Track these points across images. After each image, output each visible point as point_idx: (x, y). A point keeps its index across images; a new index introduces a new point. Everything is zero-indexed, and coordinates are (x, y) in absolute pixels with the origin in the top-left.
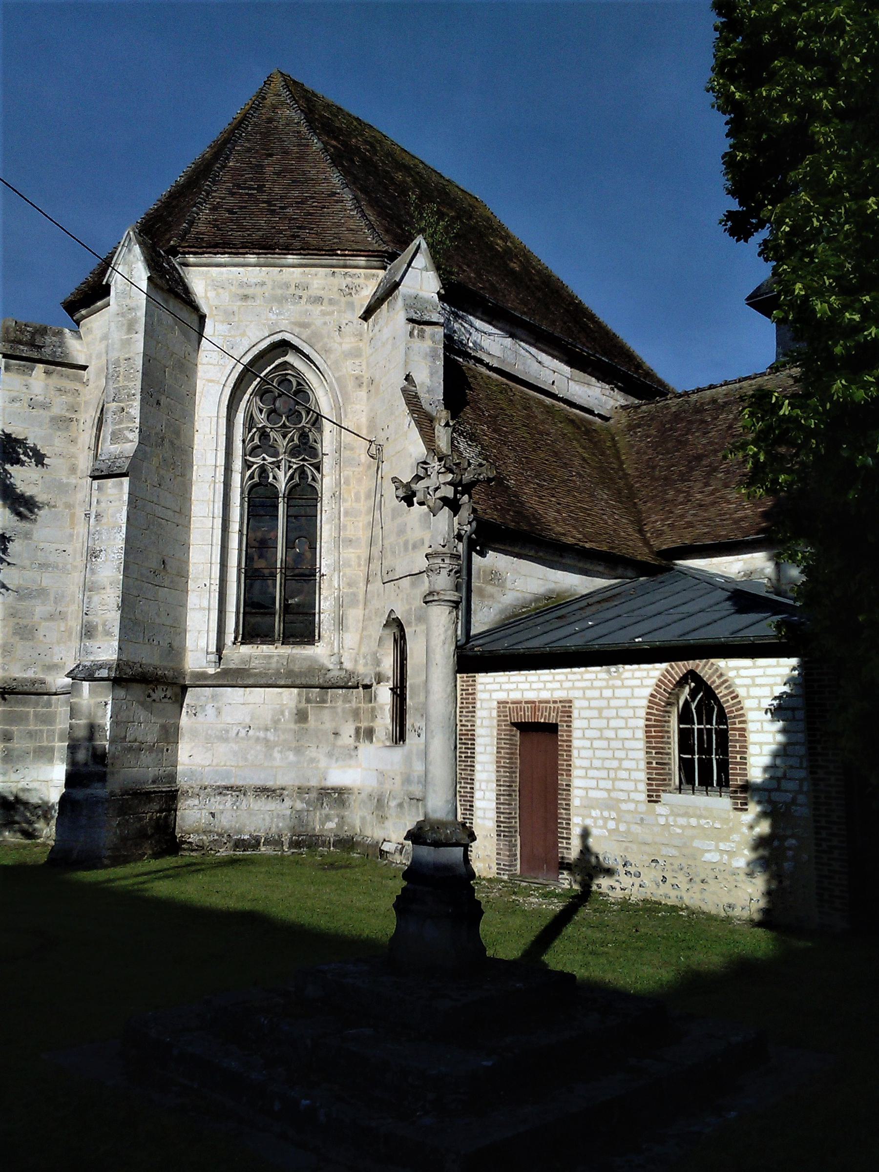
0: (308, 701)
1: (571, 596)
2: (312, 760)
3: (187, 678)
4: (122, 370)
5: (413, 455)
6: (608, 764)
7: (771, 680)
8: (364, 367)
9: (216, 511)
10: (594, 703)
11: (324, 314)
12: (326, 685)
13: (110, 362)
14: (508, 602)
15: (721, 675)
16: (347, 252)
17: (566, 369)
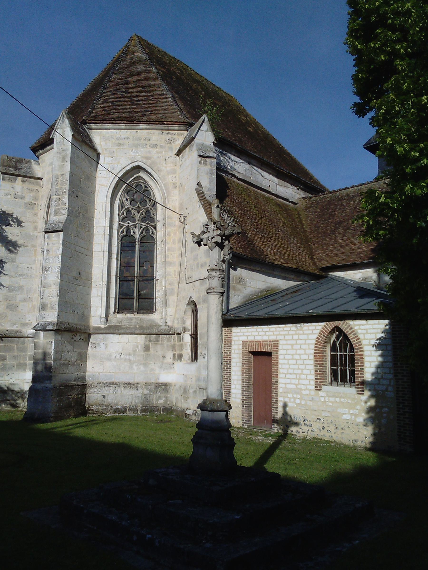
0: (150, 341)
2: (152, 370)
3: (91, 330)
4: (59, 180)
6: (296, 371)
7: (376, 331)
8: (177, 178)
10: (289, 342)
11: (158, 152)
12: (159, 333)
14: (247, 293)
15: (351, 328)
16: (169, 123)
17: (276, 180)
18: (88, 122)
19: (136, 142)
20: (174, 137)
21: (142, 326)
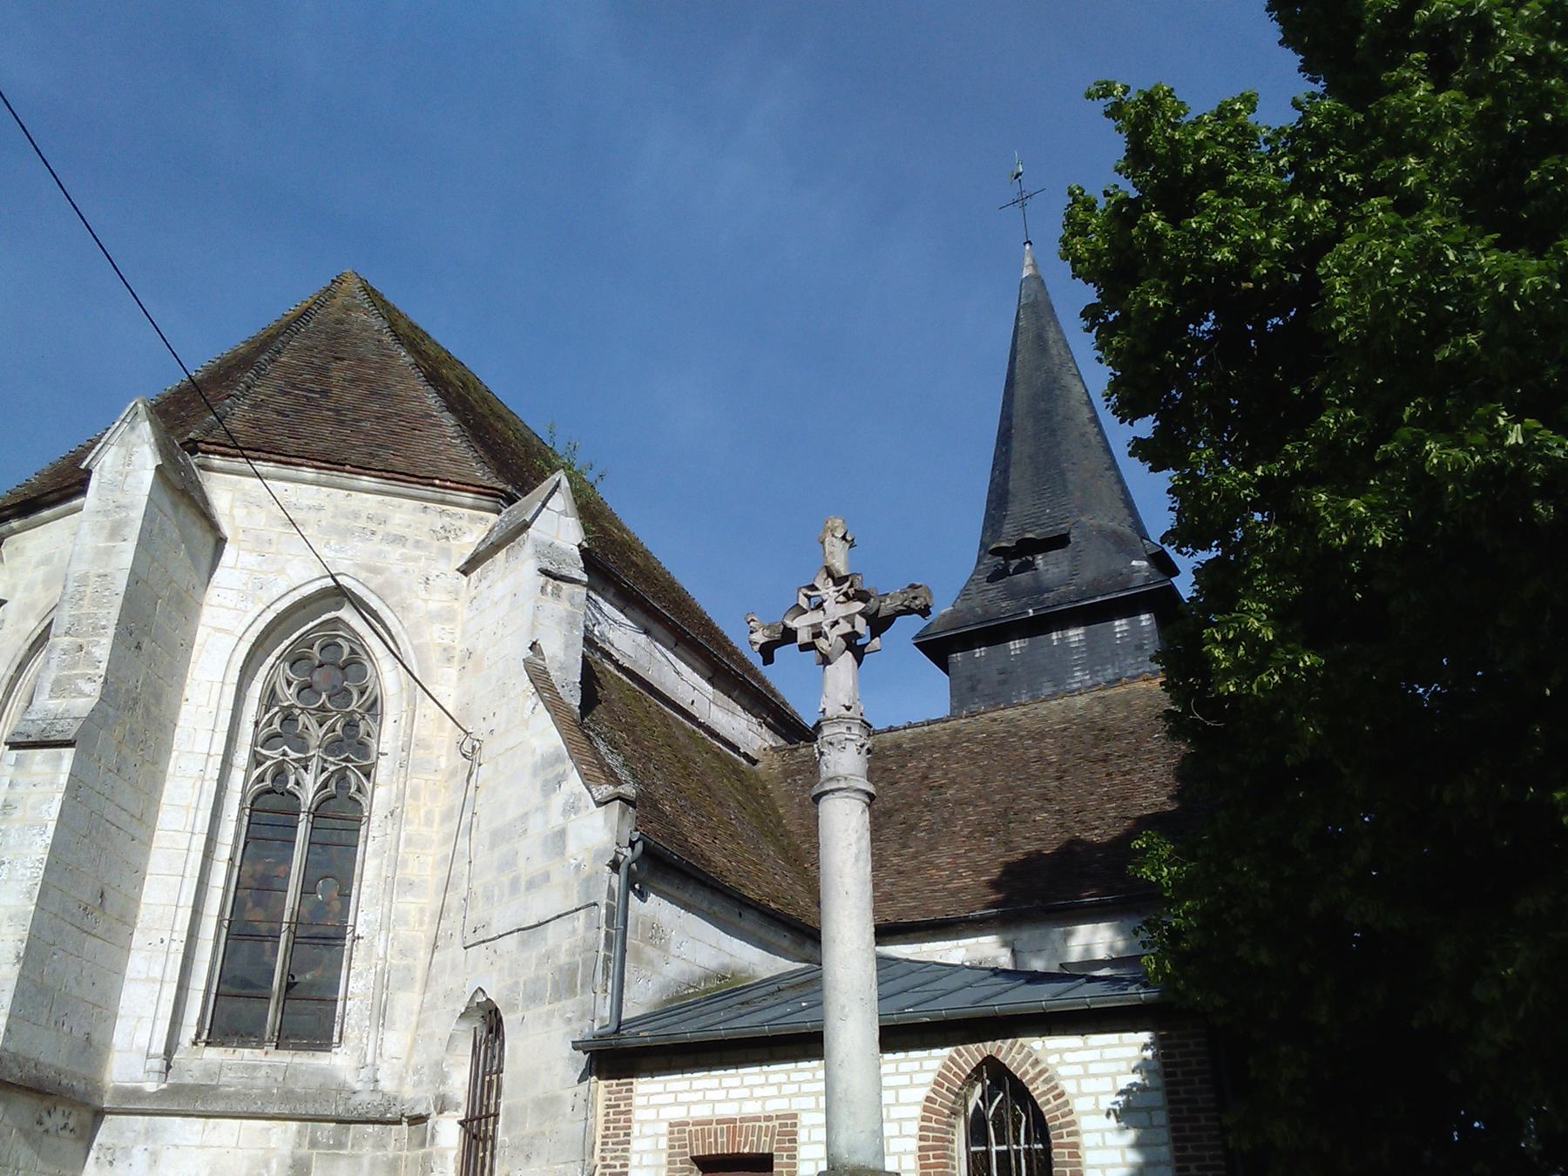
0: (314, 1144)
1: (748, 978)
3: (107, 1097)
4: (89, 590)
5: (538, 751)
7: (1112, 1067)
8: (458, 635)
9: (198, 824)
11: (405, 558)
12: (347, 1116)
13: (71, 578)
14: (671, 975)
15: (1037, 1062)
18: (203, 446)
19: (343, 522)
20: (458, 523)
21: (292, 1092)
